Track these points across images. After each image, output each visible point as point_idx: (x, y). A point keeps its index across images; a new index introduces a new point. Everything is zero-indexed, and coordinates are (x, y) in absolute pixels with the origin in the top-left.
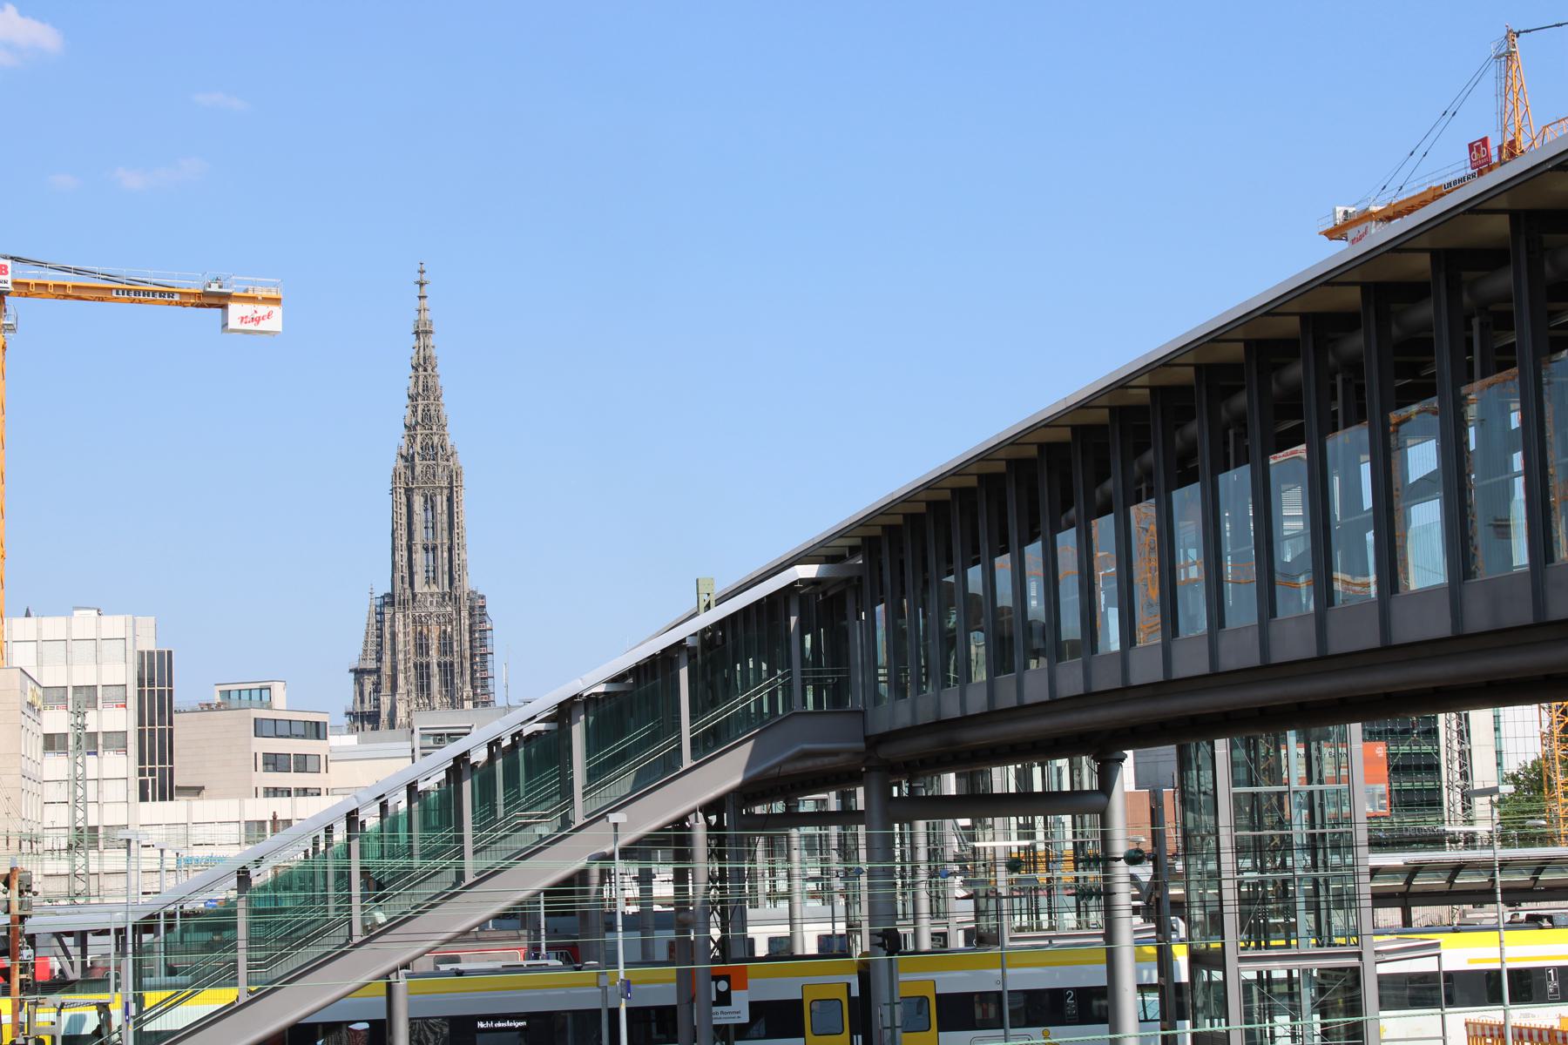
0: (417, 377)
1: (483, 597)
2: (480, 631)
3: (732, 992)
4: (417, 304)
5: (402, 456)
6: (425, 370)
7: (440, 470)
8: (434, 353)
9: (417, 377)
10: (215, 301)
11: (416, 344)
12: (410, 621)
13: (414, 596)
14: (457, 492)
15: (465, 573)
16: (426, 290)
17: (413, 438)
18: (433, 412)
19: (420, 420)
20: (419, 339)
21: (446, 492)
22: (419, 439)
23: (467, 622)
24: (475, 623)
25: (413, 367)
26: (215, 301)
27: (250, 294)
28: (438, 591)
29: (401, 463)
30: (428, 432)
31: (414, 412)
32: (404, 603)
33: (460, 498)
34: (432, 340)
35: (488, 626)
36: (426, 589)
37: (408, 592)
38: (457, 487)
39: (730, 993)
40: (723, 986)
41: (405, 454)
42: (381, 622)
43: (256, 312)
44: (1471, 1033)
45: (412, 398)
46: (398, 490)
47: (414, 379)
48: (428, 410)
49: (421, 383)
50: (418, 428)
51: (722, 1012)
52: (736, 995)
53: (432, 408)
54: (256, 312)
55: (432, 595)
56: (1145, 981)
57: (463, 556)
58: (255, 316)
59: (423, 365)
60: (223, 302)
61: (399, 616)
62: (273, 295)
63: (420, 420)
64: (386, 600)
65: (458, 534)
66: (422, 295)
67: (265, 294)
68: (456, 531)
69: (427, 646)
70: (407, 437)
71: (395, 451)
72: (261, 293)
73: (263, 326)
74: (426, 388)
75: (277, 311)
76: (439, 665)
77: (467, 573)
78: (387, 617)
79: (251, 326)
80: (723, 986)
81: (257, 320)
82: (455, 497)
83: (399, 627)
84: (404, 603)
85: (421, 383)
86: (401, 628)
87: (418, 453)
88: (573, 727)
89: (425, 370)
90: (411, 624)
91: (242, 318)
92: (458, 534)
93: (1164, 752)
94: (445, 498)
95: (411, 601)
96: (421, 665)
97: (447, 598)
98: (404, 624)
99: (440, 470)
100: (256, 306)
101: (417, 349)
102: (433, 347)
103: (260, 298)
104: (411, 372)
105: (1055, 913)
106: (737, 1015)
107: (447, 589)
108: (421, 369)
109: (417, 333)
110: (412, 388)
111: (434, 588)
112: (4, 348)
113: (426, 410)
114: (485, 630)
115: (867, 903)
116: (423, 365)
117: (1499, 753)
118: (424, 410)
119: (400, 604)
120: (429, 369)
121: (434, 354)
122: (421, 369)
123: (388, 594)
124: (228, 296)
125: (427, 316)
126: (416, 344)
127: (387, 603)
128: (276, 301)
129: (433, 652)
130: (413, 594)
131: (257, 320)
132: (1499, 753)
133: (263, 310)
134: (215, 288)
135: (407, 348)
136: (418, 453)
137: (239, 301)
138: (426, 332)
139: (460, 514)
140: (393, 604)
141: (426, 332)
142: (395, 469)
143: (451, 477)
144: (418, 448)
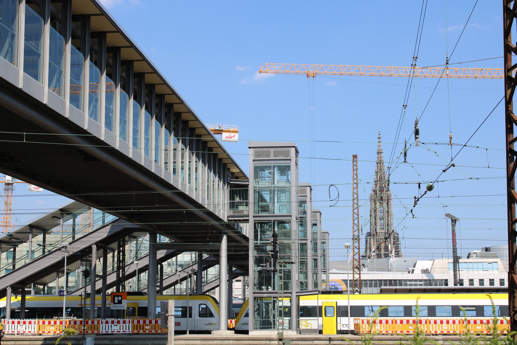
0: (378, 166)
1: (398, 234)
2: (397, 244)
3: (122, 300)
5: (373, 190)
6: (380, 164)
7: (385, 195)
8: (383, 159)
9: (378, 166)
10: (218, 132)
11: (378, 156)
12: (375, 240)
13: (377, 233)
14: (390, 201)
15: (392, 227)
17: (376, 185)
18: (382, 177)
19: (379, 180)
20: (379, 155)
21: (386, 201)
22: (378, 185)
23: (393, 241)
24: (395, 242)
25: (377, 163)
26: (218, 132)
27: (229, 130)
28: (384, 232)
29: (373, 193)
30: (381, 183)
31: (377, 178)
33: (391, 203)
34: (382, 155)
35: (399, 243)
36: (380, 231)
37: (375, 232)
38: (390, 200)
39: (122, 301)
40: (120, 298)
41: (374, 190)
42: (366, 241)
43: (230, 135)
44: (205, 316)
45: (377, 173)
46: (372, 201)
47: (377, 167)
48: (381, 176)
49: (379, 168)
50: (378, 182)
51: (119, 306)
53: (382, 176)
54: (230, 135)
55: (382, 233)
57: (391, 221)
58: (230, 136)
60: (221, 133)
62: (236, 130)
63: (379, 180)
64: (368, 234)
65: (390, 214)
66: (379, 141)
67: (233, 130)
68: (389, 213)
69: (381, 248)
70: (375, 185)
71: (372, 188)
72: (232, 129)
73: (233, 139)
74: (380, 169)
75: (237, 135)
76: (384, 254)
77: (393, 226)
78: (368, 240)
79: (229, 139)
80: (120, 298)
81: (231, 137)
82: (389, 203)
83: (372, 243)
85: (379, 168)
86: (372, 243)
87: (378, 190)
89: (380, 164)
90: (376, 242)
91: (226, 137)
92: (390, 214)
94: (386, 203)
95: (375, 235)
96: (379, 254)
97: (387, 234)
98: (373, 242)
99: (385, 195)
100: (230, 133)
101: (378, 158)
102: (383, 157)
103: (231, 131)
104: (376, 165)
106: (123, 307)
107: (387, 231)
108: (379, 164)
109: (378, 153)
110: (376, 170)
111: (383, 231)
112: (395, 183)
113: (380, 176)
114: (398, 244)
115: (316, 305)
118: (380, 176)
119: (372, 236)
120: (382, 164)
121: (383, 160)
122: (379, 164)
123: (369, 232)
124: (222, 131)
125: (381, 148)
126: (378, 156)
127: (368, 235)
128: (237, 132)
129: (382, 250)
130: (376, 232)
131: (231, 137)
134: (218, 128)
136: (378, 190)
137: (225, 132)
139: (391, 208)
140: (370, 236)
141: (381, 153)
142: (371, 194)
143: (388, 197)
144: (378, 188)
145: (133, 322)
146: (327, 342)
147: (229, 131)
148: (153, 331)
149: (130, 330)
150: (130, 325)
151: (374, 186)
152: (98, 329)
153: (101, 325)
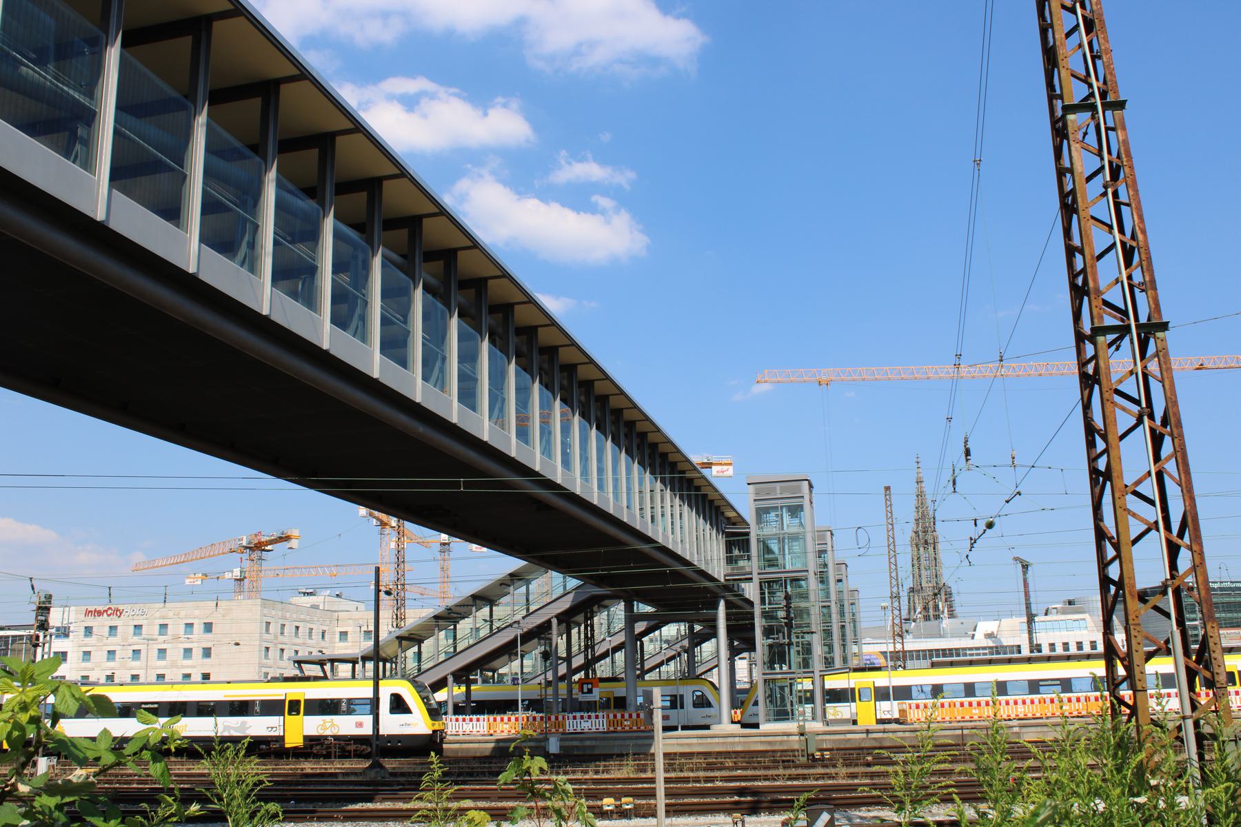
4: (917, 470)
16: (920, 465)
17: (918, 524)
32: (918, 591)
34: (923, 485)
36: (927, 585)
40: (590, 686)
52: (594, 690)
56: (349, 675)
59: (920, 495)
61: (916, 597)
67: (726, 462)
73: (726, 474)
74: (922, 504)
75: (731, 468)
79: (721, 474)
80: (590, 686)
83: (917, 601)
84: (918, 591)
88: (1005, 644)
93: (1234, 641)
105: (589, 665)
111: (930, 585)
116: (920, 495)
117: (954, 470)
124: (711, 464)
125: (921, 475)
128: (730, 464)
129: (931, 611)
132: (954, 470)
133: (725, 468)
134: (706, 461)
135: (913, 488)
138: (921, 482)
141: (921, 482)
145: (608, 717)
146: (864, 736)
147: (721, 464)
148: (635, 728)
149: (605, 727)
150: (605, 720)
151: (915, 526)
152: (563, 726)
153: (567, 721)
